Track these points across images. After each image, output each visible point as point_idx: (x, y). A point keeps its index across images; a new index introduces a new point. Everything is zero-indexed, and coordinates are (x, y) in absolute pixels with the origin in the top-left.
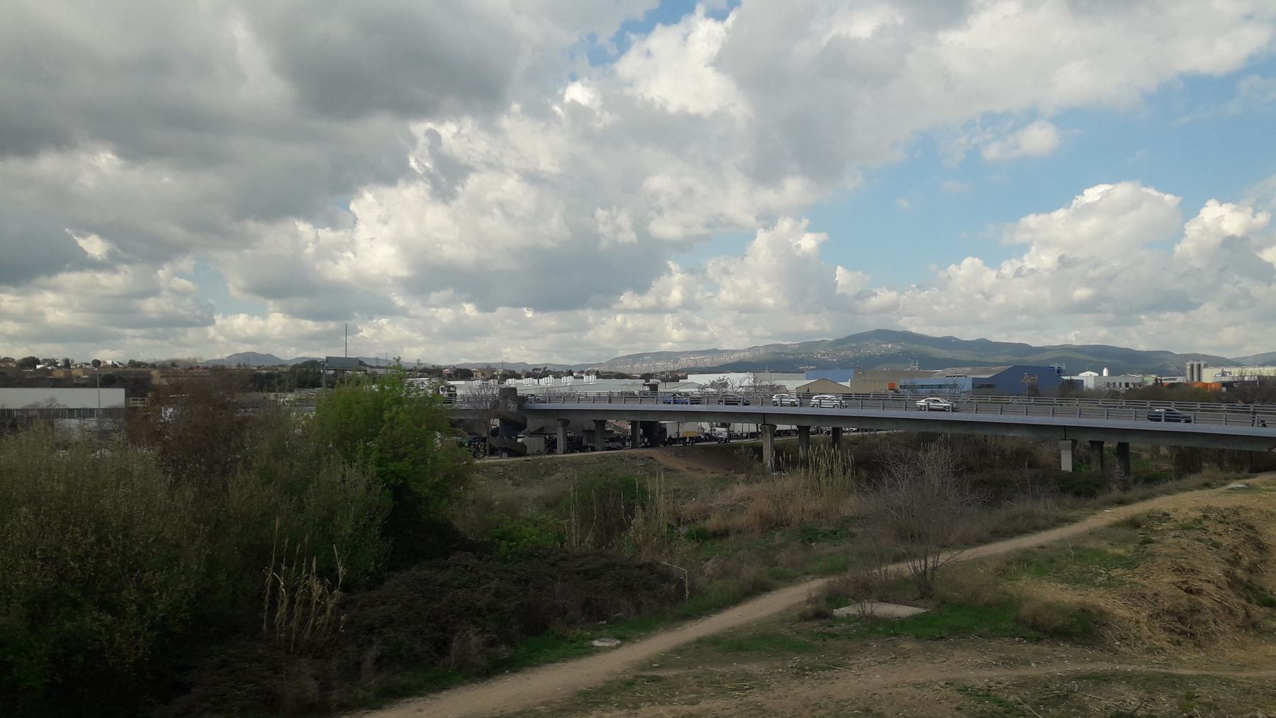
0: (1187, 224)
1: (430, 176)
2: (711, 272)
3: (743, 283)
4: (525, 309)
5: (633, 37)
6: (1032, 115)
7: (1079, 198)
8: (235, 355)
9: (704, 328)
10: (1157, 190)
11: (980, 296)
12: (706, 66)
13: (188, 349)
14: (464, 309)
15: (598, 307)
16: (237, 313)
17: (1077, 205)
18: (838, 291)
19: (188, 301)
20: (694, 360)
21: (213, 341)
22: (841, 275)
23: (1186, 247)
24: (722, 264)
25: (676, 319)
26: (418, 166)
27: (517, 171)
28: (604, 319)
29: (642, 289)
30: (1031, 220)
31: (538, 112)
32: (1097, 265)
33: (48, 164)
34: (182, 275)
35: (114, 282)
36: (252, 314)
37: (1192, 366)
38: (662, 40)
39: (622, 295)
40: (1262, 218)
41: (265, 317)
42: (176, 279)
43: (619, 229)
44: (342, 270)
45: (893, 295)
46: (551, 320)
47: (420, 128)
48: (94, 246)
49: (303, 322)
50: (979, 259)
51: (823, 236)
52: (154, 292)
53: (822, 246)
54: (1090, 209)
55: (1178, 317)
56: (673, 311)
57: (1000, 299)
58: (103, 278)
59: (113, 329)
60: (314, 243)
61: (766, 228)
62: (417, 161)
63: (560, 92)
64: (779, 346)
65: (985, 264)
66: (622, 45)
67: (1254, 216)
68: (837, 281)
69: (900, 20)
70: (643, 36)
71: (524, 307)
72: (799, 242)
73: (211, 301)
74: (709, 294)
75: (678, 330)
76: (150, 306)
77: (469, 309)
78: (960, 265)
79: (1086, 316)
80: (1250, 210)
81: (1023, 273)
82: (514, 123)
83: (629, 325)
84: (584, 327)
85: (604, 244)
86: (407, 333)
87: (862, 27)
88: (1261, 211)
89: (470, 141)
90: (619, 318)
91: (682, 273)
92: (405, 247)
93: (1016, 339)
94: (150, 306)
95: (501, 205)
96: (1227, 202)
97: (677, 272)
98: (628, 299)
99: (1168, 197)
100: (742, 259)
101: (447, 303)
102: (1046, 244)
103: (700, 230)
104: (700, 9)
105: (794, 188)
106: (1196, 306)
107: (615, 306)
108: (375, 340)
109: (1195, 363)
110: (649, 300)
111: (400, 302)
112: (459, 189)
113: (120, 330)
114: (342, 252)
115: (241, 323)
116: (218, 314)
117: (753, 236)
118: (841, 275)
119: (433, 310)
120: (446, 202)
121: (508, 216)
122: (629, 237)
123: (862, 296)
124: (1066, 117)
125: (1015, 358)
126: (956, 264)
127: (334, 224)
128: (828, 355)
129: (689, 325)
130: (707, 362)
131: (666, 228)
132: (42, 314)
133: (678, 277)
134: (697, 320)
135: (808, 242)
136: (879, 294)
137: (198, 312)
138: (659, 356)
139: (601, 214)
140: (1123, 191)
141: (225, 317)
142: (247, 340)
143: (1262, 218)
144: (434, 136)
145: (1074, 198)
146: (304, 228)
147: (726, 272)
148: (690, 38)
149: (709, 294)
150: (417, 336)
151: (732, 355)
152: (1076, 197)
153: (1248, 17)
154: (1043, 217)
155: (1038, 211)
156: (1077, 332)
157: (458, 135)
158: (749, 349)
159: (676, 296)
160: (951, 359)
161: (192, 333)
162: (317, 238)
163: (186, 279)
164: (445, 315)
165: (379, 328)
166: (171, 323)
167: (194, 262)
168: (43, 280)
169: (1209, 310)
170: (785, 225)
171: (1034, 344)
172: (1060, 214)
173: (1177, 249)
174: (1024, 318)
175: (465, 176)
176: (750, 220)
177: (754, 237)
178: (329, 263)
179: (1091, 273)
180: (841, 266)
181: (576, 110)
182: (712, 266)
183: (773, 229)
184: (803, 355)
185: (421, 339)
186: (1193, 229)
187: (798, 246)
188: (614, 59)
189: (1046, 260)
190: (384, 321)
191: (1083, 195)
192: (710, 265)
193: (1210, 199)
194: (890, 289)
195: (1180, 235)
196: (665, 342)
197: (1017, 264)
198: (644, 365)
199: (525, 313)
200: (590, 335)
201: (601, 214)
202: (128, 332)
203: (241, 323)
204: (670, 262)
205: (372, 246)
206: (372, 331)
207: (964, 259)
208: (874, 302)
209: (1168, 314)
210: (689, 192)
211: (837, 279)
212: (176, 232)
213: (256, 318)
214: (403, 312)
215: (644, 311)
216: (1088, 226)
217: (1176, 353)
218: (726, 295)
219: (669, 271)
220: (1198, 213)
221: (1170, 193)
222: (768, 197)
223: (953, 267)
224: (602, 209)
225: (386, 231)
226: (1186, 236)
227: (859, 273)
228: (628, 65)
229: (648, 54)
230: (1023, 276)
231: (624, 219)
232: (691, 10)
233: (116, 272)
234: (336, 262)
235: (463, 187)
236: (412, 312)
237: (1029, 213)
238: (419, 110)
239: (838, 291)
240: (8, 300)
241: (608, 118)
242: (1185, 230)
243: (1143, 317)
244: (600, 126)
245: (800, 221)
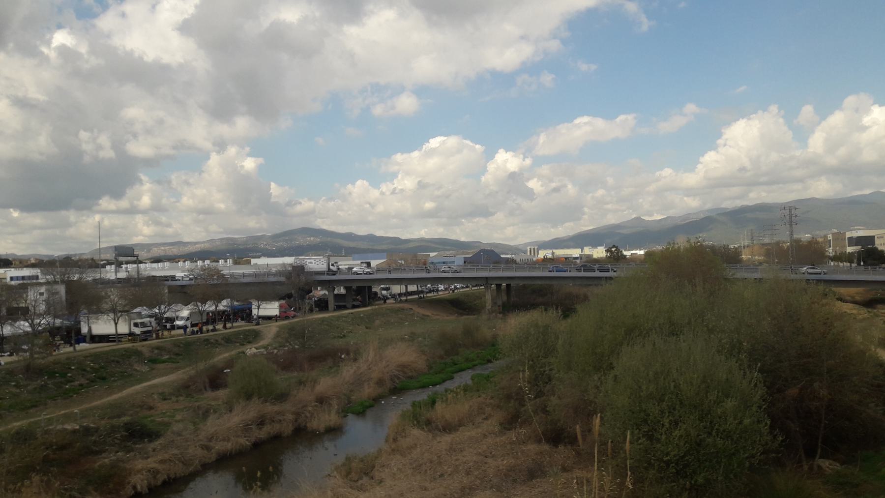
0: (488, 164)
2: (174, 183)
3: (200, 192)
4: (11, 210)
7: (427, 144)
9: (169, 225)
10: (472, 142)
11: (368, 206)
15: (79, 208)
18: (273, 200)
20: (164, 250)
23: (487, 178)
24: (184, 178)
27: (8, 97)
29: (118, 195)
30: (399, 157)
37: (530, 249)
39: (101, 199)
43: (100, 147)
45: (312, 204)
46: (36, 219)
50: (367, 181)
51: (261, 160)
53: (260, 167)
54: (432, 152)
55: (483, 221)
56: (144, 212)
57: (380, 208)
61: (218, 152)
63: (48, 36)
64: (232, 239)
65: (370, 185)
67: (524, 160)
68: (271, 193)
71: (11, 208)
72: (243, 164)
74: (173, 200)
78: (354, 184)
79: (431, 220)
80: (522, 156)
81: (397, 191)
83: (106, 223)
84: (68, 225)
87: (290, 15)
88: (528, 157)
90: (97, 217)
91: (151, 183)
93: (391, 234)
96: (510, 151)
97: (147, 182)
98: (106, 203)
99: (478, 146)
100: (200, 174)
102: (408, 173)
105: (242, 125)
106: (492, 214)
107: (96, 208)
109: (532, 248)
110: (124, 204)
117: (208, 158)
122: (108, 153)
123: (289, 204)
124: (421, 91)
125: (393, 247)
126: (352, 184)
128: (269, 246)
129: (158, 223)
130: (175, 251)
131: (140, 149)
133: (147, 186)
134: (164, 219)
135: (250, 164)
136: (303, 202)
139: (84, 135)
140: (452, 141)
143: (528, 161)
145: (424, 144)
147: (187, 183)
148: (158, 7)
149: (173, 200)
151: (195, 245)
152: (425, 144)
153: (523, 38)
154: (405, 156)
155: (402, 153)
156: (426, 230)
159: (146, 200)
160: (354, 248)
169: (500, 216)
170: (232, 151)
171: (403, 238)
172: (416, 154)
173: (483, 179)
174: (395, 220)
176: (208, 145)
177: (209, 158)
179: (437, 193)
180: (274, 182)
181: (63, 50)
182: (175, 178)
183: (223, 153)
184: (250, 245)
186: (491, 167)
187: (242, 167)
188: (95, 16)
189: (408, 183)
193: (501, 148)
194: (310, 199)
195: (484, 170)
196: (137, 236)
197: (392, 187)
199: (12, 213)
200: (71, 231)
201: (84, 135)
204: (140, 174)
208: (299, 208)
209: (477, 219)
210: (161, 122)
211: (271, 191)
215: (119, 212)
216: (433, 162)
217: (484, 242)
218: (186, 201)
219: (141, 182)
221: (479, 144)
222: (223, 129)
224: (85, 130)
226: (488, 171)
227: (287, 188)
229: (123, 15)
230: (396, 193)
231: (104, 139)
239: (273, 200)
241: (94, 61)
242: (487, 167)
243: (463, 220)
245: (243, 149)
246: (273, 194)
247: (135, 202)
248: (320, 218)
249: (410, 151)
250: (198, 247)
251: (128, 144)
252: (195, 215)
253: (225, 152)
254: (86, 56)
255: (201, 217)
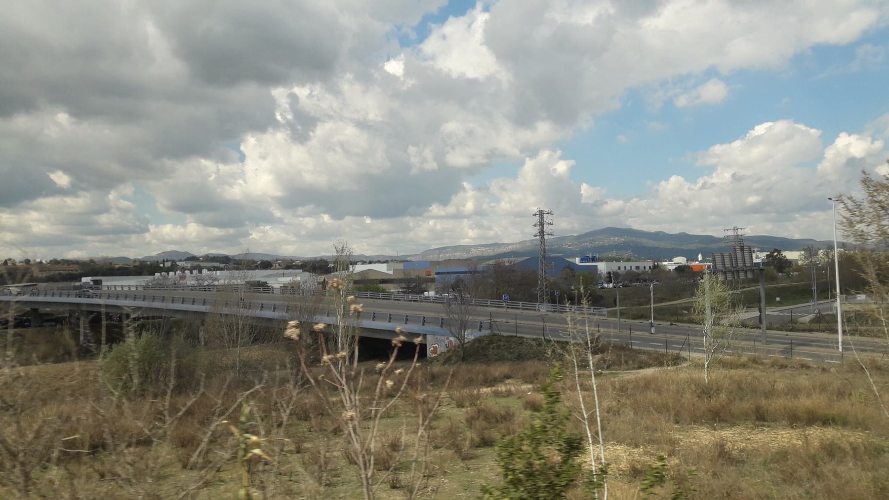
1: (290, 125)
3: (516, 197)
5: (433, 26)
6: (711, 73)
8: (164, 253)
9: (490, 228)
11: (681, 203)
12: (481, 45)
13: (132, 249)
14: (323, 218)
15: (413, 215)
16: (166, 223)
17: (749, 137)
18: (583, 201)
19: (130, 216)
20: (481, 251)
21: (149, 243)
22: (585, 189)
23: (825, 166)
25: (471, 222)
26: (282, 118)
27: (352, 120)
28: (420, 223)
29: (445, 201)
30: (717, 149)
31: (365, 79)
32: (759, 180)
33: (21, 122)
34: (125, 198)
35: (78, 203)
36: (175, 223)
38: (453, 27)
40: (878, 144)
41: (184, 226)
42: (121, 201)
43: (424, 160)
44: (235, 192)
46: (383, 224)
47: (279, 93)
48: (61, 179)
49: (211, 229)
51: (572, 162)
52: (106, 210)
53: (571, 170)
54: (758, 139)
56: (468, 217)
57: (696, 205)
58: (69, 201)
59: (80, 237)
60: (216, 174)
61: (531, 157)
62: (281, 114)
65: (685, 180)
66: (423, 33)
67: (872, 143)
69: (612, 11)
70: (440, 25)
73: (147, 215)
75: (472, 230)
76: (104, 219)
77: (326, 218)
78: (668, 181)
79: (757, 215)
80: (869, 139)
82: (348, 86)
83: (438, 227)
85: (414, 171)
86: (283, 235)
87: (588, 17)
88: (877, 140)
89: (319, 100)
90: (431, 223)
92: (280, 176)
94: (104, 219)
95: (342, 144)
98: (435, 209)
99: (813, 131)
101: (310, 214)
103: (480, 160)
104: (479, 6)
105: (544, 129)
108: (262, 241)
111: (278, 214)
112: (311, 134)
113: (84, 237)
114: (236, 180)
115: (168, 230)
116: (152, 224)
117: (523, 163)
118: (585, 189)
119: (301, 219)
120: (302, 143)
121: (347, 152)
122: (432, 165)
125: (703, 246)
126: (665, 180)
127: (224, 160)
129: (479, 226)
131: (457, 159)
132: (30, 226)
133: (470, 193)
134: (486, 223)
135: (562, 167)
136: (609, 202)
137: (137, 223)
138: (457, 248)
139: (412, 149)
140: (781, 126)
141: (157, 226)
142: (173, 242)
143: (878, 144)
144: (294, 98)
145: (747, 133)
146: (207, 164)
147: (503, 189)
150: (292, 238)
152: (749, 132)
154: (725, 146)
155: (722, 143)
157: (310, 96)
158: (520, 243)
159: (470, 206)
161: (134, 238)
162: (218, 170)
163: (129, 201)
164: (310, 222)
165: (264, 232)
166: (119, 231)
167: (133, 189)
168: (26, 203)
170: (545, 155)
172: (737, 144)
173: (819, 167)
174: (713, 217)
175: (315, 126)
176: (516, 152)
178: (227, 187)
179: (756, 186)
180: (585, 183)
181: (391, 79)
183: (536, 158)
185: (294, 239)
186: (830, 153)
187: (555, 170)
189: (723, 177)
190: (268, 227)
191: (754, 130)
192: (493, 184)
195: (821, 157)
196: (464, 239)
198: (447, 255)
200: (411, 235)
201: (412, 149)
202: (89, 238)
203: (168, 230)
205: (256, 175)
206: (260, 235)
207: (670, 177)
209: (815, 213)
212: (116, 168)
213: (179, 226)
214: (280, 221)
215: (448, 217)
216: (757, 152)
219: (464, 188)
220: (834, 142)
222: (526, 135)
223: (663, 183)
224: (413, 146)
225: (266, 164)
226: (825, 158)
227: (598, 188)
228: (430, 45)
229: (444, 37)
231: (428, 153)
232: (473, 6)
233: (77, 196)
234: (231, 186)
235: (313, 132)
236: (286, 221)
237: (714, 144)
238: (271, 79)
239: (583, 201)
240: (6, 218)
241: (411, 83)
243: (797, 216)
244: (405, 88)
246: (583, 195)
247: (461, 208)
248: (631, 217)
249: (730, 141)
250: (509, 249)
251: (448, 156)
252: (512, 217)
253: (537, 157)
254: (402, 79)
255: (518, 219)
